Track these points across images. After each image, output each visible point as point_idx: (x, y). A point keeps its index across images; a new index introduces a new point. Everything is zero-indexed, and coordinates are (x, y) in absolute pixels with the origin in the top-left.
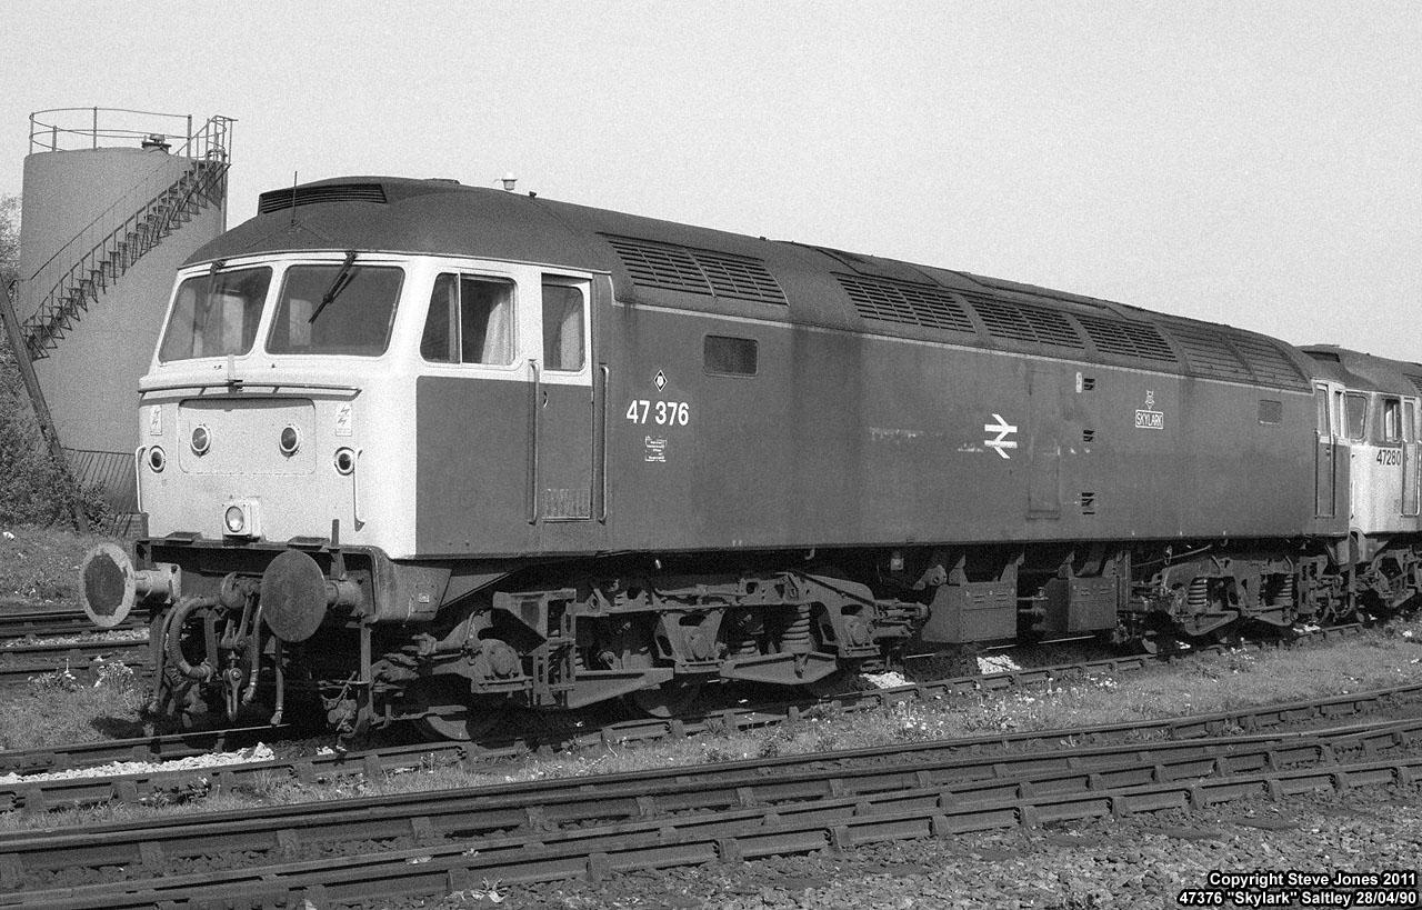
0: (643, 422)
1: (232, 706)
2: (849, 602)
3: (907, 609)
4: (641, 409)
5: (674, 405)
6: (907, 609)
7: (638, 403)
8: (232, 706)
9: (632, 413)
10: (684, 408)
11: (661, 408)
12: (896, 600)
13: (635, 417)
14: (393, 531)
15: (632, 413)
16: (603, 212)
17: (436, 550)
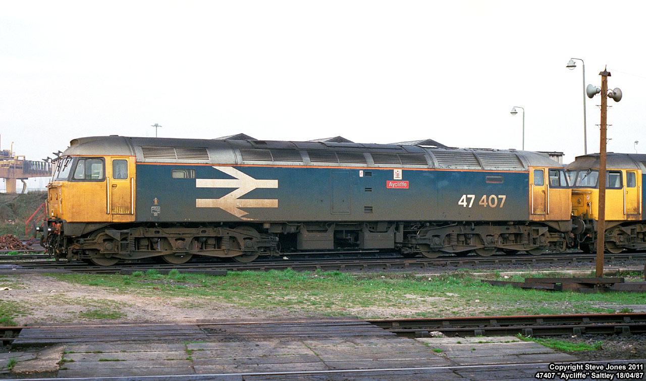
4: (468, 200)
5: (473, 197)
7: (467, 197)
9: (463, 201)
13: (465, 204)
15: (463, 201)
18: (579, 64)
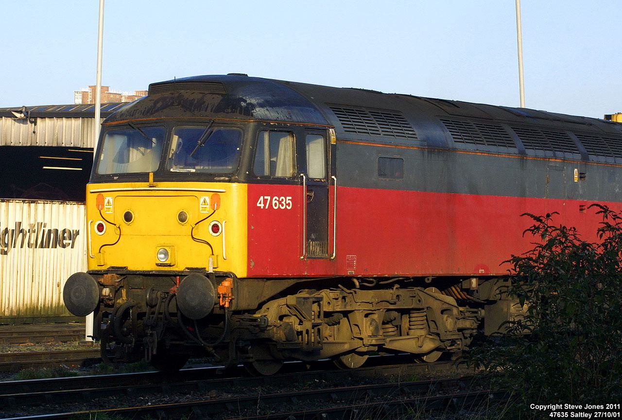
0: (267, 207)
1: (148, 355)
2: (445, 306)
3: (473, 312)
4: (265, 201)
5: (269, 198)
6: (473, 312)
8: (148, 355)
9: (260, 203)
10: (276, 199)
11: (283, 200)
12: (467, 307)
13: (262, 205)
14: (237, 263)
15: (260, 203)
16: (288, 83)
17: (260, 273)
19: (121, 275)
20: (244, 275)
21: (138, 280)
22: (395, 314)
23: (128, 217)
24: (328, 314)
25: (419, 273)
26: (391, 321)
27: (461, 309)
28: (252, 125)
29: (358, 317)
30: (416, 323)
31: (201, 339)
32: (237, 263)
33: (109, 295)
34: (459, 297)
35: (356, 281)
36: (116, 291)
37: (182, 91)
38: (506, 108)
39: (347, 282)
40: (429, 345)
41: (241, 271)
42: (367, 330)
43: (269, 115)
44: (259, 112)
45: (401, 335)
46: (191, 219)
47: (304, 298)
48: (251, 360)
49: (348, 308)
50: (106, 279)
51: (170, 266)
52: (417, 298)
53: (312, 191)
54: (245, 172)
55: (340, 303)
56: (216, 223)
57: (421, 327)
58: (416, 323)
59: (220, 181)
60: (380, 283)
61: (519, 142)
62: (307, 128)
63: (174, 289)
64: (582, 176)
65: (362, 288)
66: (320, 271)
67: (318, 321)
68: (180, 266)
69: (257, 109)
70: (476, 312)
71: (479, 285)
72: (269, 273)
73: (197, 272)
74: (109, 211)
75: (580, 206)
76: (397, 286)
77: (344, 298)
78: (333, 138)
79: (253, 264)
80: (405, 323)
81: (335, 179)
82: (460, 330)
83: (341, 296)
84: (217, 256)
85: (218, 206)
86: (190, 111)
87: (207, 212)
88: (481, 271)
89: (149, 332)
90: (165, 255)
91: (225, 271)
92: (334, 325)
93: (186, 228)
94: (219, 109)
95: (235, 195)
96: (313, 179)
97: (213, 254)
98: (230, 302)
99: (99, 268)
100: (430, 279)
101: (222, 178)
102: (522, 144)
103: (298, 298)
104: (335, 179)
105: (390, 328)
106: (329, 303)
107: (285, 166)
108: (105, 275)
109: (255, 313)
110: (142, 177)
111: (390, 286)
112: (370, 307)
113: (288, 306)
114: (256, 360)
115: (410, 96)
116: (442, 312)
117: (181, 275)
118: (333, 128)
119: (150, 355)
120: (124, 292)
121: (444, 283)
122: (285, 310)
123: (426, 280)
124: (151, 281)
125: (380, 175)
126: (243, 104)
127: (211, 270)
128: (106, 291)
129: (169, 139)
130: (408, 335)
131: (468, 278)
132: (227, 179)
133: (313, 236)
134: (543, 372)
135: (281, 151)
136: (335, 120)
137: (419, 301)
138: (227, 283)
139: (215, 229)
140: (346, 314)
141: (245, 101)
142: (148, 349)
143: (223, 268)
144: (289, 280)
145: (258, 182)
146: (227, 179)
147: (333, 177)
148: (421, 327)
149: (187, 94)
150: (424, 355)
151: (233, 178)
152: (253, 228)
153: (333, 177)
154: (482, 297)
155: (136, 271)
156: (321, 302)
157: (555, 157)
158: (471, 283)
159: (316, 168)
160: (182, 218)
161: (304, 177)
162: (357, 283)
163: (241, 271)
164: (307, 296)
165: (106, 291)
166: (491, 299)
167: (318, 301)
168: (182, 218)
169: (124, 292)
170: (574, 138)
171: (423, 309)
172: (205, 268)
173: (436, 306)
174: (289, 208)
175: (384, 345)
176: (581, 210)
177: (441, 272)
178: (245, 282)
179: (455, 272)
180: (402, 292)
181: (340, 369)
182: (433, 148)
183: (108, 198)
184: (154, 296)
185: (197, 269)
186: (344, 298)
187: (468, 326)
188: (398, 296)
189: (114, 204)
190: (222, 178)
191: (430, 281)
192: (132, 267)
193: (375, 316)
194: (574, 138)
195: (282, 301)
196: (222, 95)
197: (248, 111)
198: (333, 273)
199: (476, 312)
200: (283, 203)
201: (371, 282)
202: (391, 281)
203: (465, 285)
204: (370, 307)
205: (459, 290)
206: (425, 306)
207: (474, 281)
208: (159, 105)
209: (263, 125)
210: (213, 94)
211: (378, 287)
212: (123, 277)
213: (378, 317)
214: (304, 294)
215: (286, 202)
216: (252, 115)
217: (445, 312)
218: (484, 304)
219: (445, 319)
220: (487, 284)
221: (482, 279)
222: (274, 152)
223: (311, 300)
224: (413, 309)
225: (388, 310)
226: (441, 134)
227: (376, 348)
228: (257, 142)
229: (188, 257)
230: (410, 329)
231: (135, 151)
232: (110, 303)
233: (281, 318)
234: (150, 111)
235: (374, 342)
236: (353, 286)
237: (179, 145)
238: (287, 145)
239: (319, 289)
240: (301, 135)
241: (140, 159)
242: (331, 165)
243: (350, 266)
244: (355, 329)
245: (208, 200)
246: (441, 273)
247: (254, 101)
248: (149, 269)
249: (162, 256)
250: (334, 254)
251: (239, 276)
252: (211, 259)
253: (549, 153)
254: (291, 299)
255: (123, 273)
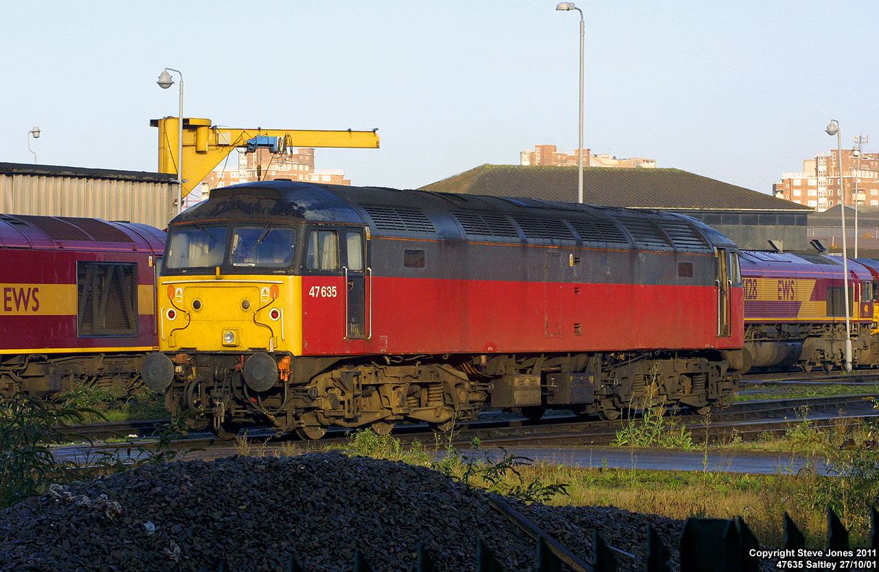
3: (484, 386)
4: (316, 290)
5: (318, 288)
6: (484, 386)
13: (313, 294)
14: (294, 346)
17: (311, 352)
18: (176, 78)
19: (191, 355)
20: (300, 354)
21: (206, 359)
22: (418, 387)
23: (197, 305)
24: (365, 387)
25: (438, 351)
26: (414, 393)
27: (472, 383)
28: (303, 225)
29: (388, 390)
30: (434, 396)
31: (263, 408)
32: (294, 346)
33: (181, 372)
34: (470, 372)
35: (386, 358)
36: (187, 369)
37: (240, 196)
38: (433, 190)
39: (379, 359)
40: (445, 416)
41: (296, 350)
42: (395, 401)
43: (317, 217)
44: (309, 215)
45: (420, 406)
46: (254, 305)
47: (347, 373)
48: (303, 426)
49: (380, 382)
50: (180, 358)
51: (235, 346)
52: (436, 373)
53: (352, 281)
54: (299, 266)
55: (373, 377)
56: (276, 309)
57: (439, 399)
58: (434, 396)
59: (278, 274)
60: (407, 360)
61: (520, 231)
62: (347, 227)
63: (239, 366)
64: (576, 261)
65: (392, 364)
66: (359, 350)
67: (357, 392)
68: (244, 346)
69: (308, 212)
70: (486, 386)
71: (488, 361)
72: (319, 352)
73: (259, 352)
74: (179, 300)
75: (576, 288)
76: (419, 362)
77: (376, 373)
78: (368, 234)
79: (306, 344)
80: (424, 396)
81: (371, 270)
82: (471, 402)
83: (374, 371)
84: (277, 338)
85: (277, 295)
86: (249, 214)
87: (267, 301)
88: (490, 349)
89: (218, 403)
90: (231, 338)
91: (283, 350)
92: (367, 396)
93: (249, 315)
94: (274, 212)
95: (291, 285)
96: (352, 271)
97: (273, 336)
98: (289, 377)
99: (170, 349)
100: (447, 356)
101: (280, 272)
102: (524, 233)
103: (342, 372)
104: (371, 270)
105: (413, 401)
106: (365, 377)
107: (329, 261)
108: (177, 355)
109: (305, 386)
110: (210, 271)
111: (413, 363)
112: (396, 381)
113: (333, 380)
114: (307, 426)
115: (375, 187)
116: (456, 386)
117: (246, 354)
118: (368, 226)
119: (219, 423)
120: (194, 369)
121: (457, 360)
122: (331, 383)
123: (443, 357)
124: (218, 360)
125: (406, 265)
126: (295, 208)
127: (272, 350)
128: (179, 369)
129: (231, 238)
130: (427, 406)
131: (479, 355)
132: (284, 272)
133: (353, 320)
134: (99, 491)
135: (326, 247)
136: (368, 219)
137: (438, 376)
138: (286, 360)
139: (275, 314)
140: (377, 386)
141: (297, 205)
142: (217, 418)
143: (281, 348)
144: (334, 358)
145: (309, 274)
146: (284, 272)
147: (369, 268)
148: (439, 399)
149: (245, 199)
150: (442, 424)
151: (289, 271)
152: (306, 313)
153: (369, 268)
154: (490, 372)
155: (205, 352)
156: (360, 376)
157: (553, 244)
158: (480, 360)
159: (355, 261)
160: (245, 306)
161: (346, 269)
162: (388, 360)
163: (296, 350)
164: (347, 371)
165: (179, 369)
166: (498, 374)
167: (357, 375)
168: (245, 306)
169: (194, 369)
170: (569, 226)
171: (440, 383)
172: (265, 348)
173: (451, 381)
174: (334, 296)
175: (408, 414)
176: (576, 292)
177: (456, 351)
178: (299, 360)
179: (468, 350)
180: (423, 368)
181: (301, 440)
182: (450, 242)
183: (178, 289)
184: (221, 372)
185: (259, 349)
186: (376, 373)
187: (478, 399)
188: (420, 371)
189: (184, 293)
190: (280, 272)
191: (447, 358)
192: (201, 348)
193: (401, 389)
194: (569, 226)
195: (328, 375)
196: (276, 200)
197: (299, 214)
198: (370, 351)
199: (486, 386)
200: (330, 292)
201: (399, 359)
202: (415, 358)
203: (476, 362)
204: (396, 381)
205: (470, 366)
206: (442, 380)
207: (483, 357)
208: (220, 208)
209: (314, 226)
210: (268, 199)
211: (404, 364)
212: (192, 357)
213: (405, 390)
214: (345, 369)
215: (331, 291)
216: (304, 217)
217: (459, 386)
218: (491, 379)
219: (458, 393)
220: (494, 360)
221: (491, 355)
222: (320, 247)
223: (353, 374)
224: (432, 383)
225: (412, 384)
226: (454, 228)
227: (402, 417)
228: (307, 240)
229: (251, 338)
230: (428, 401)
231: (194, 246)
232: (182, 379)
233: (327, 390)
234: (214, 213)
235: (401, 412)
236: (384, 363)
237: (239, 243)
238: (330, 241)
239: (356, 365)
240: (342, 232)
241: (198, 254)
242: (367, 260)
243: (383, 345)
244: (385, 401)
245: (268, 290)
246: (456, 350)
247: (303, 205)
248: (216, 350)
249: (229, 338)
250: (370, 335)
251: (295, 355)
252: (271, 340)
253: (548, 241)
254: (336, 373)
255: (194, 354)
